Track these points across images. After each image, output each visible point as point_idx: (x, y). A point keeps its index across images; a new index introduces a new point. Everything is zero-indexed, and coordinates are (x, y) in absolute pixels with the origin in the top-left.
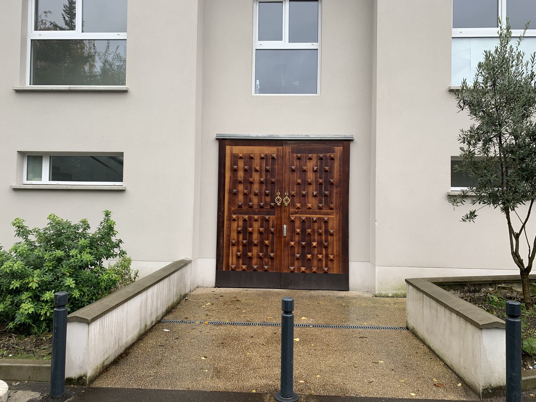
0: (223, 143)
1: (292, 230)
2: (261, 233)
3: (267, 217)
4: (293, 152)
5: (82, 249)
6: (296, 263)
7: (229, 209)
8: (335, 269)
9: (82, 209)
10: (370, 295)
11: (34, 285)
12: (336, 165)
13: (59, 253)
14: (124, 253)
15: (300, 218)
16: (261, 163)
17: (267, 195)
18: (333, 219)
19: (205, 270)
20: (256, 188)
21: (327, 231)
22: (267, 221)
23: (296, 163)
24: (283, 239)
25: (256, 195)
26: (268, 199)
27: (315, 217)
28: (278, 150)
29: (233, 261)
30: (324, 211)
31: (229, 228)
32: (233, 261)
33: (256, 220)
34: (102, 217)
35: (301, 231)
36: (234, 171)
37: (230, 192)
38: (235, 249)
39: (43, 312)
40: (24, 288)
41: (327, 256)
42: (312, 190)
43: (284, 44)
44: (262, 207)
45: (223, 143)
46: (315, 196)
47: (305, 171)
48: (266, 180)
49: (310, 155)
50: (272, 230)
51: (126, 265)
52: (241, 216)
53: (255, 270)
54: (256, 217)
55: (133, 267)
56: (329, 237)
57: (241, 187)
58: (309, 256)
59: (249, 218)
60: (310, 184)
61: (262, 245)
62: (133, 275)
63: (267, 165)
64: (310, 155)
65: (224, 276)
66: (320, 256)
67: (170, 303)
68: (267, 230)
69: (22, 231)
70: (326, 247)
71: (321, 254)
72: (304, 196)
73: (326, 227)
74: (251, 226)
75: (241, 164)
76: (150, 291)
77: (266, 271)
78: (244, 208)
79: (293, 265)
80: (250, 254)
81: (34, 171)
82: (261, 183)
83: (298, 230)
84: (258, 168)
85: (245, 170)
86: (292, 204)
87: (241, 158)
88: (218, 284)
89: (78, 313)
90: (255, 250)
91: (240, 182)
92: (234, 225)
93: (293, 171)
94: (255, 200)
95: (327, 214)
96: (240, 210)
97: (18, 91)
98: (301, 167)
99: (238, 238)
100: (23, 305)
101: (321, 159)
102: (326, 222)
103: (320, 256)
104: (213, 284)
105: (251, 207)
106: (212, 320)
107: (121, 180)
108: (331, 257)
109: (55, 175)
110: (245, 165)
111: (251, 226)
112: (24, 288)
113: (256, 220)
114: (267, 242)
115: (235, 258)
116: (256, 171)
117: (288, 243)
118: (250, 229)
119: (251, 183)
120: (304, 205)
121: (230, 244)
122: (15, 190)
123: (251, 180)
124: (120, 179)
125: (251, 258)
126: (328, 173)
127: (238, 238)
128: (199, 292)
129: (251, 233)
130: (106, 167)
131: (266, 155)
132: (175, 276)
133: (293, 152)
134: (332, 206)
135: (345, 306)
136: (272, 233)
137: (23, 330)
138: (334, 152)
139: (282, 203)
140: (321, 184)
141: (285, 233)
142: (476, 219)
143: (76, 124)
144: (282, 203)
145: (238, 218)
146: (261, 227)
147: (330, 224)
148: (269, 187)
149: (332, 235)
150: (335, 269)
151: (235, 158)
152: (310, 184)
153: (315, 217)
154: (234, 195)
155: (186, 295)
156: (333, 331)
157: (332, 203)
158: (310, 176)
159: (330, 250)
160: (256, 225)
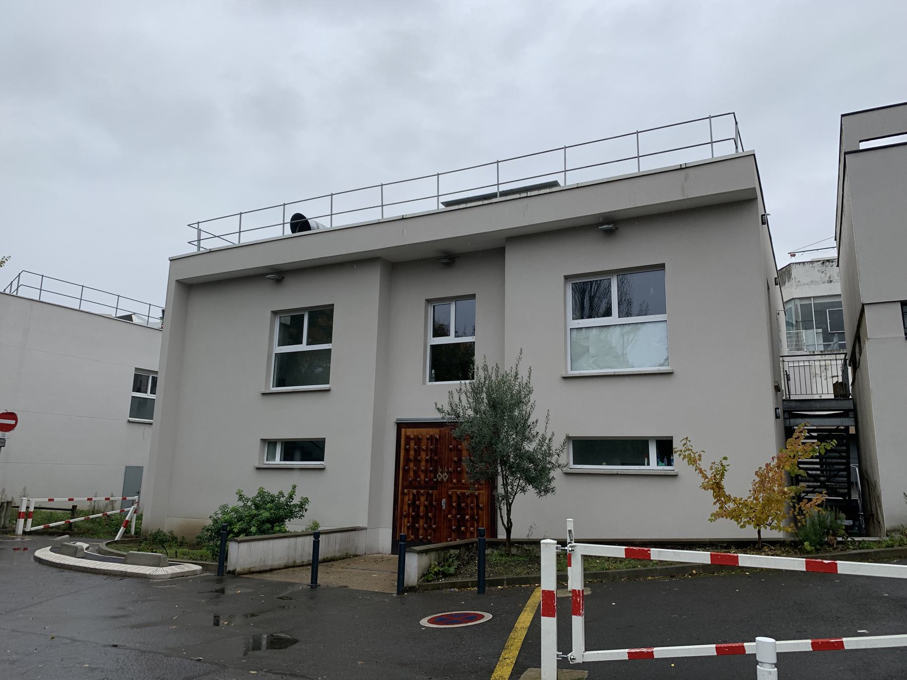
0: (401, 426)
1: (449, 504)
2: (425, 506)
7: (403, 484)
20: (423, 466)
22: (431, 495)
34: (721, 520)
37: (404, 469)
38: (406, 520)
45: (401, 426)
58: (463, 528)
59: (418, 492)
70: (478, 521)
74: (419, 500)
75: (412, 443)
82: (427, 461)
86: (450, 480)
90: (421, 522)
92: (406, 498)
93: (451, 450)
95: (479, 489)
96: (410, 486)
102: (477, 497)
103: (472, 529)
107: (323, 460)
120: (459, 481)
141: (444, 507)
143: (298, 417)
147: (481, 499)
151: (408, 439)
159: (480, 523)
160: (423, 499)
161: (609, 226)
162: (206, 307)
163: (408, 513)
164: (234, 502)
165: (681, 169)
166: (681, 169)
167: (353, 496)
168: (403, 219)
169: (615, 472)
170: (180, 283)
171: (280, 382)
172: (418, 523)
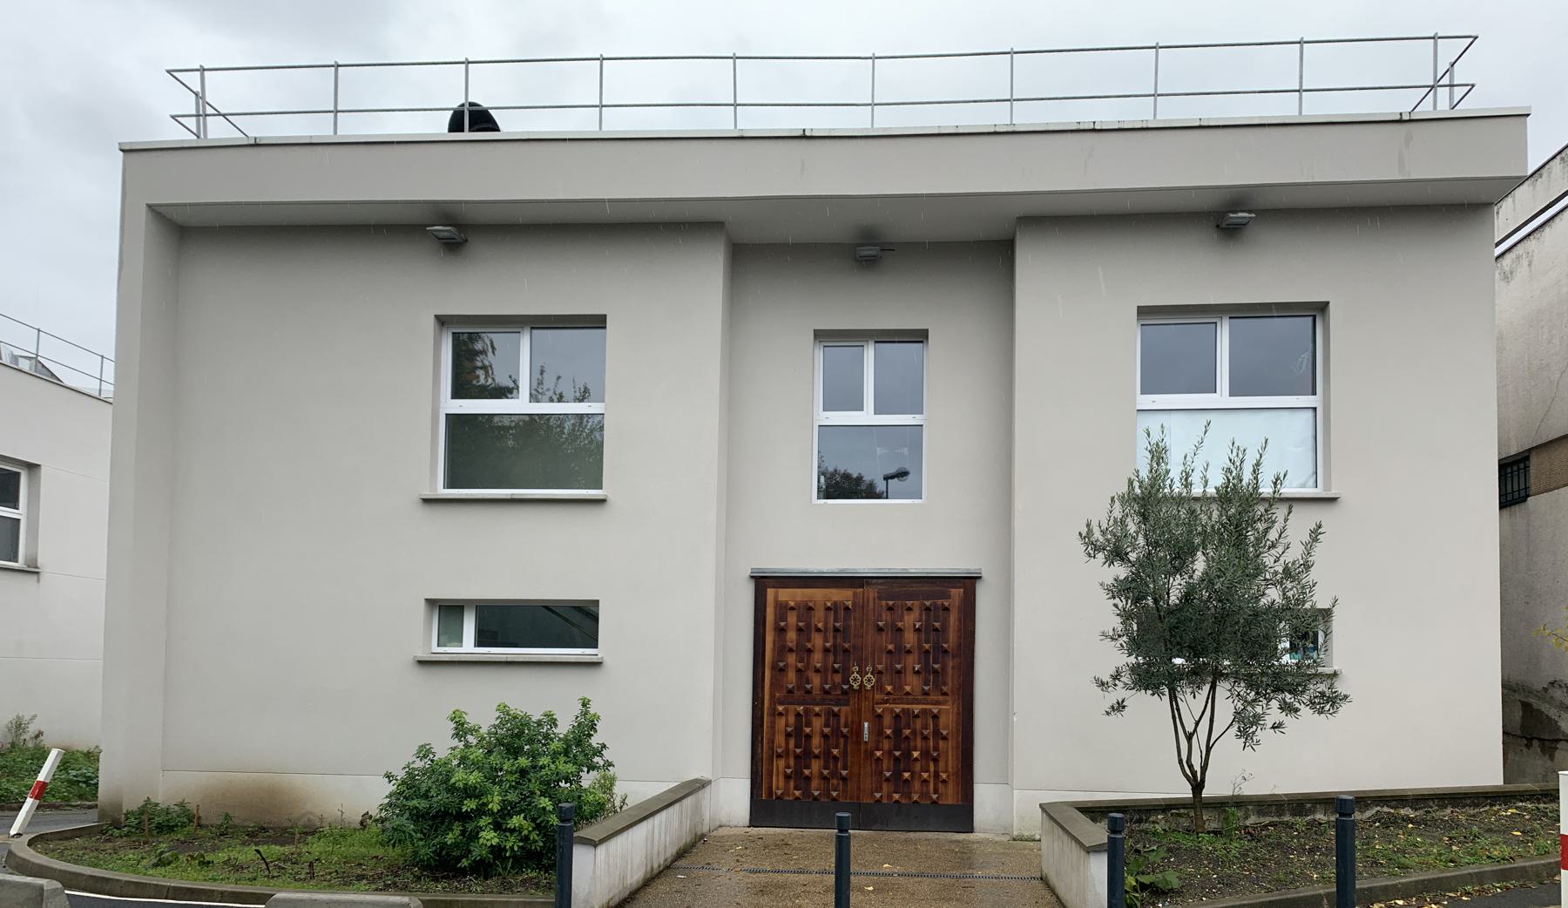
0: (763, 583)
1: (878, 732)
2: (825, 736)
3: (836, 709)
4: (880, 598)
5: (555, 756)
6: (885, 786)
7: (772, 696)
8: (950, 797)
9: (542, 693)
10: (1005, 839)
11: (495, 807)
12: (953, 618)
13: (524, 762)
14: (611, 764)
15: (892, 710)
16: (826, 618)
17: (836, 671)
18: (948, 712)
19: (731, 799)
20: (817, 659)
21: (937, 733)
22: (836, 715)
23: (886, 616)
24: (863, 747)
25: (817, 671)
26: (838, 678)
27: (917, 708)
28: (855, 595)
29: (778, 784)
30: (933, 697)
31: (773, 726)
32: (778, 784)
33: (817, 715)
34: (577, 709)
35: (894, 732)
36: (781, 631)
37: (774, 667)
38: (782, 763)
39: (509, 845)
40: (481, 811)
41: (937, 775)
42: (913, 662)
43: (867, 416)
44: (827, 692)
45: (763, 583)
46: (918, 672)
47: (900, 630)
48: (835, 646)
49: (909, 603)
50: (845, 730)
51: (607, 785)
52: (791, 707)
53: (815, 799)
54: (817, 709)
55: (619, 790)
56: (941, 743)
57: (792, 659)
58: (906, 775)
59: (806, 710)
60: (909, 652)
61: (827, 755)
62: (617, 804)
63: (836, 620)
64: (909, 603)
65: (764, 808)
66: (925, 775)
67: (682, 844)
68: (837, 732)
69: (461, 729)
70: (935, 760)
71: (927, 771)
72: (899, 672)
73: (936, 725)
74: (809, 724)
75: (792, 618)
76: (657, 818)
77: (834, 799)
78: (797, 693)
79: (879, 790)
80: (807, 772)
81: (451, 633)
82: (826, 650)
83: (889, 732)
84: (820, 625)
85: (800, 630)
86: (879, 687)
87: (792, 608)
88: (754, 822)
89: (586, 832)
90: (816, 765)
91: (791, 650)
92: (781, 722)
93: (881, 629)
94: (816, 680)
95: (938, 703)
96: (789, 697)
97: (426, 501)
98: (893, 624)
99: (787, 744)
100: (482, 834)
101: (928, 609)
102: (935, 717)
103: (925, 775)
104: (747, 822)
105: (809, 692)
106: (746, 866)
107: (595, 646)
108: (944, 776)
109: (481, 641)
110: (799, 620)
111: (809, 724)
112: (481, 811)
113: (817, 715)
114: (835, 752)
115: (781, 778)
116: (818, 630)
117: (872, 754)
118: (808, 730)
119: (810, 651)
120: (898, 688)
121: (774, 755)
122: (422, 663)
123: (809, 645)
124: (592, 642)
125: (808, 779)
126: (941, 632)
127: (787, 744)
128: (721, 832)
129: (808, 737)
130: (573, 623)
131: (835, 604)
132: (688, 801)
133: (880, 598)
134: (945, 689)
135: (965, 857)
136: (844, 736)
137: (482, 869)
138: (948, 597)
139: (862, 685)
140: (927, 652)
141: (866, 737)
142: (1126, 712)
143: (522, 552)
144: (862, 685)
145: (787, 711)
146: (827, 725)
147: (942, 720)
148: (840, 658)
149: (945, 738)
150: (950, 797)
151: (783, 609)
152: (909, 652)
153: (917, 708)
154: (780, 671)
155: (703, 836)
156: (927, 881)
157: (945, 684)
158: (910, 639)
159: (941, 764)
160: (818, 723)
161: (1228, 218)
162: (233, 288)
163: (787, 751)
164: (444, 746)
165: (1400, 121)
166: (1400, 121)
167: (673, 720)
168: (804, 137)
169: (504, 658)
170: (158, 213)
171: (451, 483)
172: (808, 767)
